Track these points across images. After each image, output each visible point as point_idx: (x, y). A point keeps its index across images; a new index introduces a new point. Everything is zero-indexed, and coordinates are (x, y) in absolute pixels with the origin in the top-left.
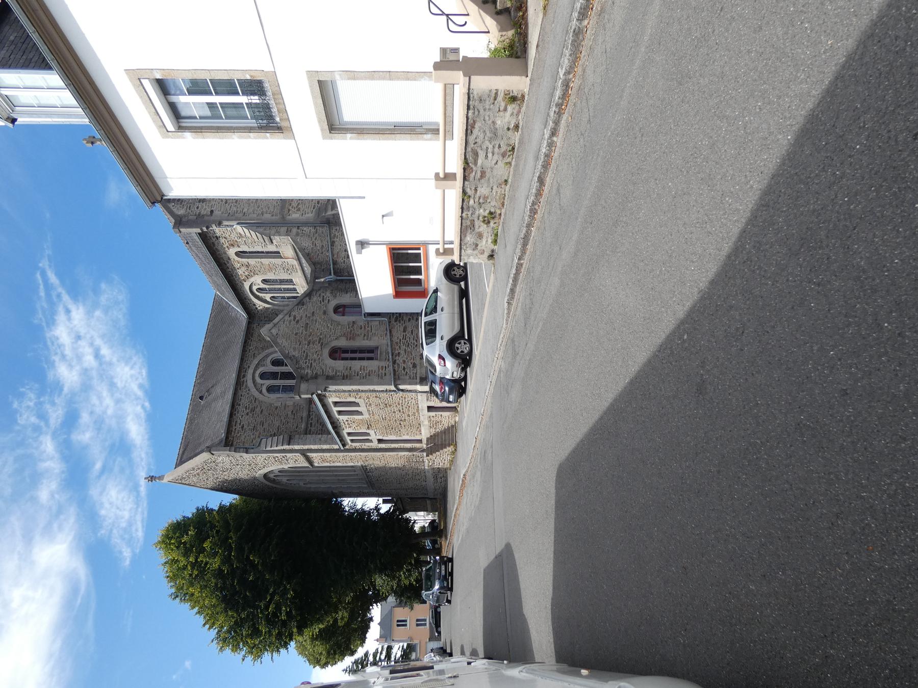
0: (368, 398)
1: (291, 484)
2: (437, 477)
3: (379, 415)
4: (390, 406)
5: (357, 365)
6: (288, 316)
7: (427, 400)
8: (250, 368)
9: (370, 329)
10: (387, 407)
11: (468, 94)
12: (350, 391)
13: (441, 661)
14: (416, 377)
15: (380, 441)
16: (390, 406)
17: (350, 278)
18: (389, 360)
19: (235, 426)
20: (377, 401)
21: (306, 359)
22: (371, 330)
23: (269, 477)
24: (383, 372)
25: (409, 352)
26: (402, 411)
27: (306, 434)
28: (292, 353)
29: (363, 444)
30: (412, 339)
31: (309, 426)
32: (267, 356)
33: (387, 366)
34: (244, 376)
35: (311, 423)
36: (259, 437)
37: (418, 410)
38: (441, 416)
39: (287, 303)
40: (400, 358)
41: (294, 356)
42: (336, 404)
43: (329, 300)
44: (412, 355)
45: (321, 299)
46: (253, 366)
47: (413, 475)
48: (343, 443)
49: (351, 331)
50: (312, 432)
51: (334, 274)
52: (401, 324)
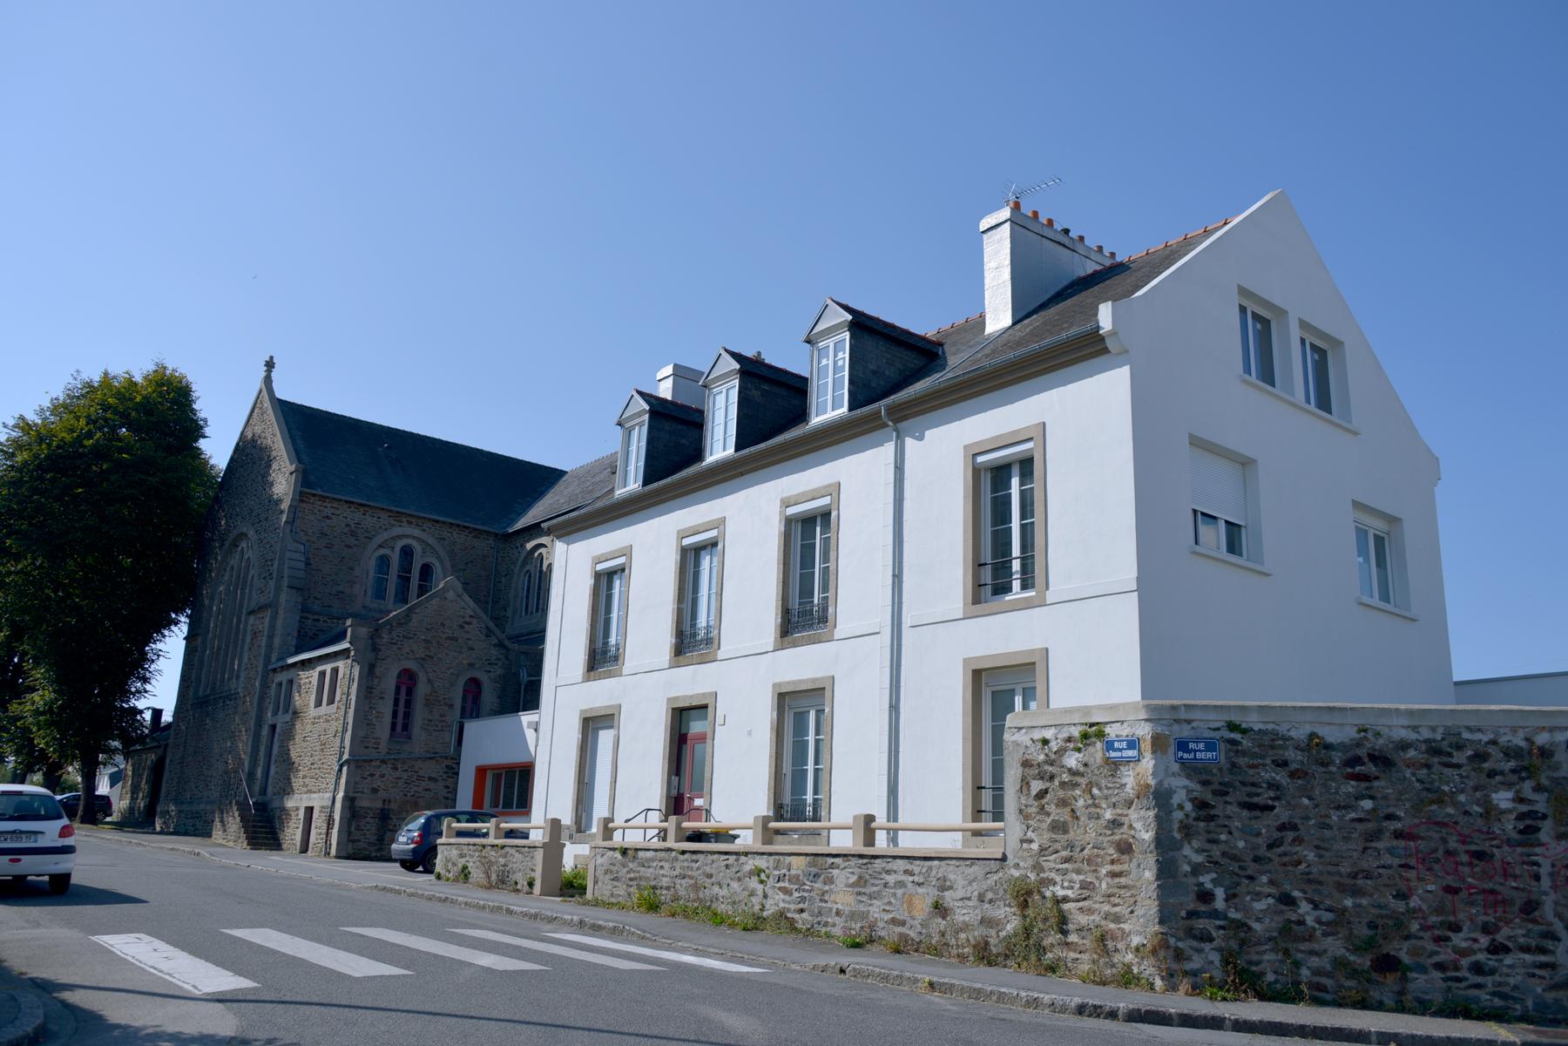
0: (337, 719)
1: (225, 570)
2: (198, 818)
3: (311, 732)
4: (322, 750)
5: (386, 708)
6: (472, 614)
7: (323, 807)
8: (421, 532)
9: (439, 728)
10: (321, 745)
11: (534, 847)
12: (348, 694)
13: (1499, 727)
14: (358, 792)
15: (274, 727)
16: (322, 750)
17: (521, 707)
18: (388, 753)
19: (332, 507)
20: (332, 731)
21: (404, 637)
22: (438, 731)
23: (242, 540)
24: (371, 745)
25: (397, 783)
26: (313, 767)
27: (302, 612)
28: (415, 619)
29: (272, 701)
30: (416, 788)
31: (316, 617)
32: (438, 557)
33: (379, 750)
34: (410, 523)
35: (318, 620)
36: (309, 541)
37: (310, 792)
38: (298, 828)
39: (520, 595)
40: (389, 769)
41: (410, 620)
42: (335, 671)
43: (490, 672)
44: (392, 787)
45: (493, 661)
46: (424, 536)
47: (208, 776)
48: (279, 670)
49: (439, 701)
50: (303, 620)
51: (530, 681)
52: (441, 774)
